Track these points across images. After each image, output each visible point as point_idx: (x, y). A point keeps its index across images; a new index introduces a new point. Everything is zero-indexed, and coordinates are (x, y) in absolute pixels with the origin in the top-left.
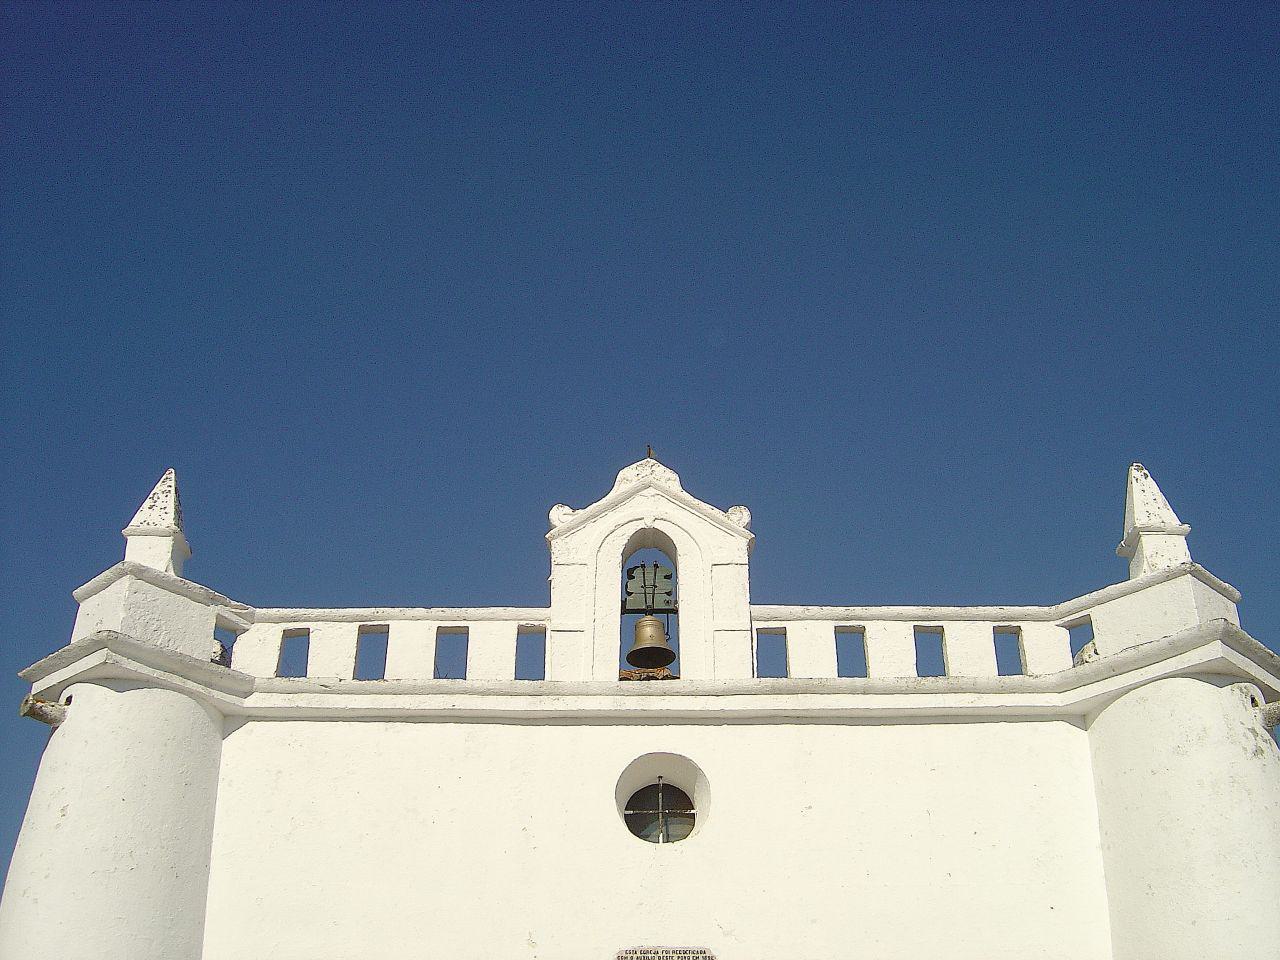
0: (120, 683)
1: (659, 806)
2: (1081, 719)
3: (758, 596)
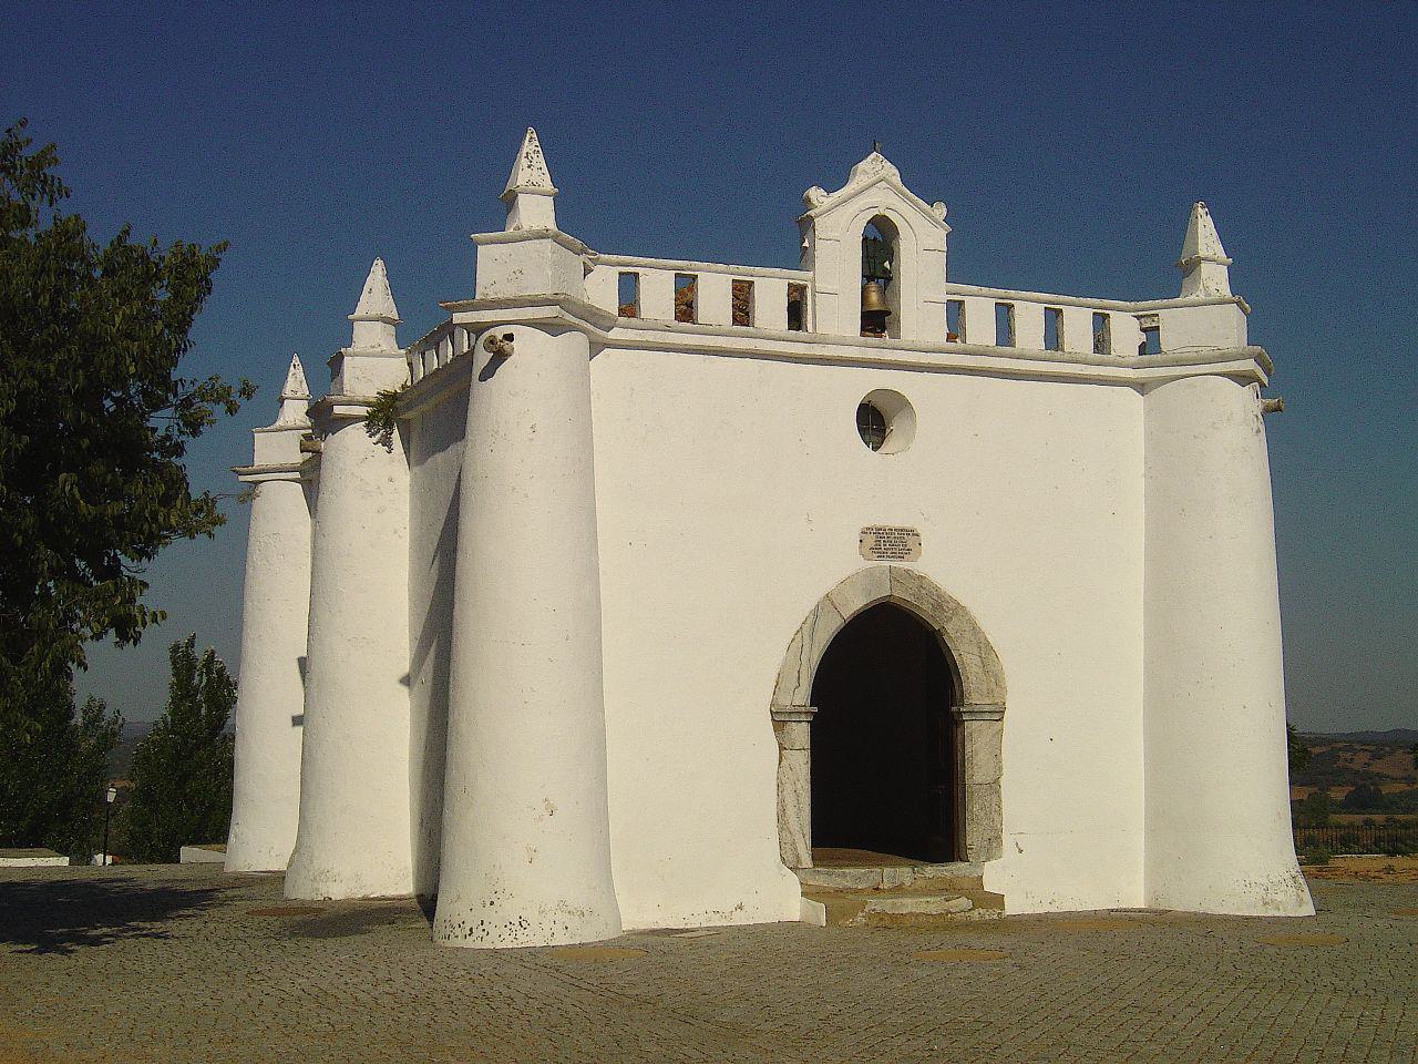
0: (553, 328)
1: (874, 421)
2: (1142, 387)
3: (951, 277)
